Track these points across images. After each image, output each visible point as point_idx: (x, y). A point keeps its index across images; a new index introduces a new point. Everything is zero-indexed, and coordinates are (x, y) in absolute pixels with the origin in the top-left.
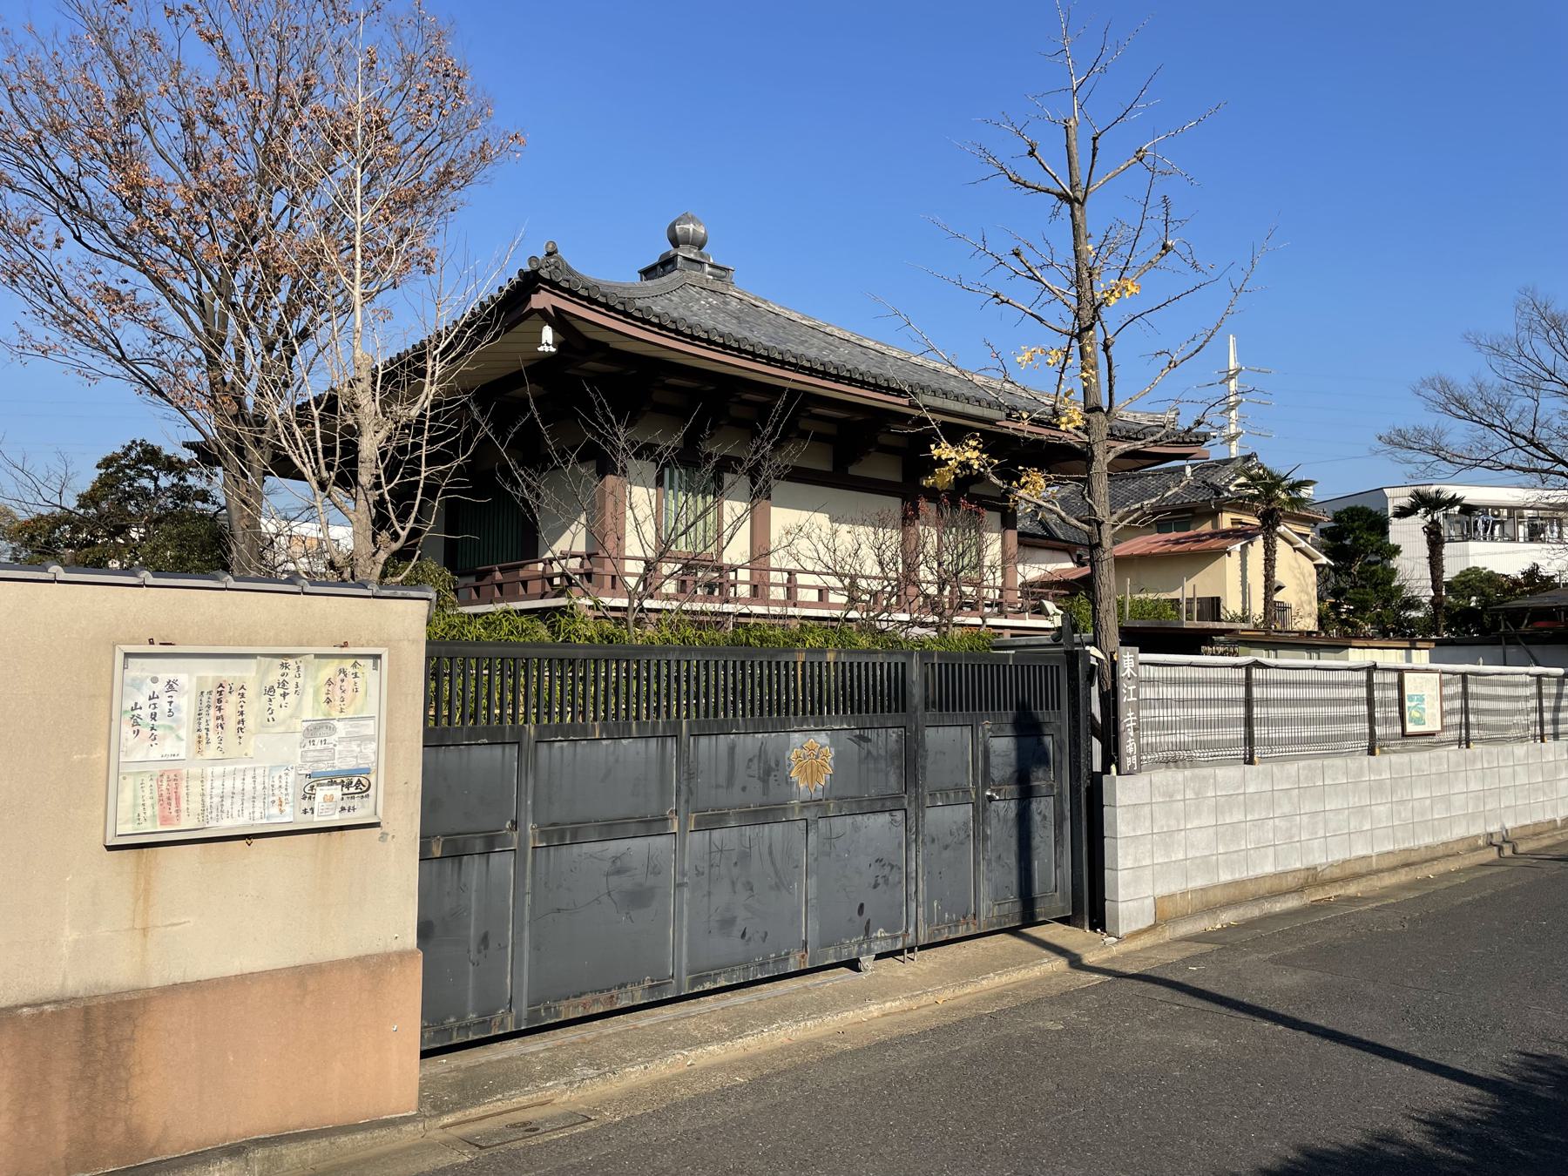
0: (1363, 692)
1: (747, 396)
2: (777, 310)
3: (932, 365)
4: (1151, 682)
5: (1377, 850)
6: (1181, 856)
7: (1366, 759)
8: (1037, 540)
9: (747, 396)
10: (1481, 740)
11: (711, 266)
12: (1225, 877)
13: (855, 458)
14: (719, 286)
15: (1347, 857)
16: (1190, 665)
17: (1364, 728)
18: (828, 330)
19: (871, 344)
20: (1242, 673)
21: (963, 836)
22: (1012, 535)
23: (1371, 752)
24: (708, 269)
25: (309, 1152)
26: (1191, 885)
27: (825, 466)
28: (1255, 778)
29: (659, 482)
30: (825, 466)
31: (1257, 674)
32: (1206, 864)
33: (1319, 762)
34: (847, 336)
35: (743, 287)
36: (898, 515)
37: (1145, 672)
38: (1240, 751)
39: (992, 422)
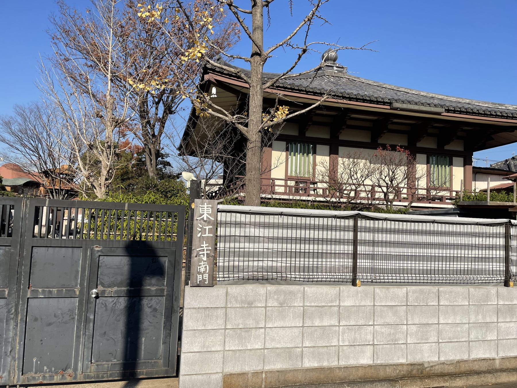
0: (502, 241)
1: (395, 120)
2: (363, 81)
3: (431, 95)
4: (226, 224)
5: (502, 354)
6: (259, 346)
7: (503, 290)
8: (496, 171)
9: (395, 120)
10: (363, 283)
11: (337, 67)
12: (309, 363)
13: (448, 143)
14: (340, 75)
15: (465, 357)
16: (477, 224)
17: (502, 267)
18: (384, 86)
19: (403, 89)
20: (351, 222)
21: (67, 318)
22: (469, 168)
23: (506, 284)
24: (335, 68)
25: (473, 380)
26: (267, 368)
27: (366, 139)
28: (350, 296)
29: (428, 163)
30: (366, 139)
31: (361, 223)
32: (288, 352)
33: (435, 289)
34: (393, 87)
35: (351, 73)
36: (285, 147)
37: (222, 217)
38: (349, 276)
39: (439, 114)
